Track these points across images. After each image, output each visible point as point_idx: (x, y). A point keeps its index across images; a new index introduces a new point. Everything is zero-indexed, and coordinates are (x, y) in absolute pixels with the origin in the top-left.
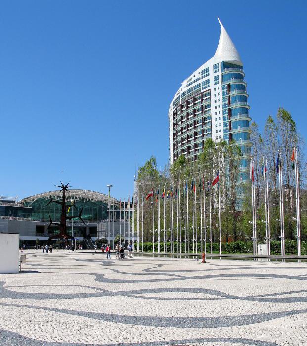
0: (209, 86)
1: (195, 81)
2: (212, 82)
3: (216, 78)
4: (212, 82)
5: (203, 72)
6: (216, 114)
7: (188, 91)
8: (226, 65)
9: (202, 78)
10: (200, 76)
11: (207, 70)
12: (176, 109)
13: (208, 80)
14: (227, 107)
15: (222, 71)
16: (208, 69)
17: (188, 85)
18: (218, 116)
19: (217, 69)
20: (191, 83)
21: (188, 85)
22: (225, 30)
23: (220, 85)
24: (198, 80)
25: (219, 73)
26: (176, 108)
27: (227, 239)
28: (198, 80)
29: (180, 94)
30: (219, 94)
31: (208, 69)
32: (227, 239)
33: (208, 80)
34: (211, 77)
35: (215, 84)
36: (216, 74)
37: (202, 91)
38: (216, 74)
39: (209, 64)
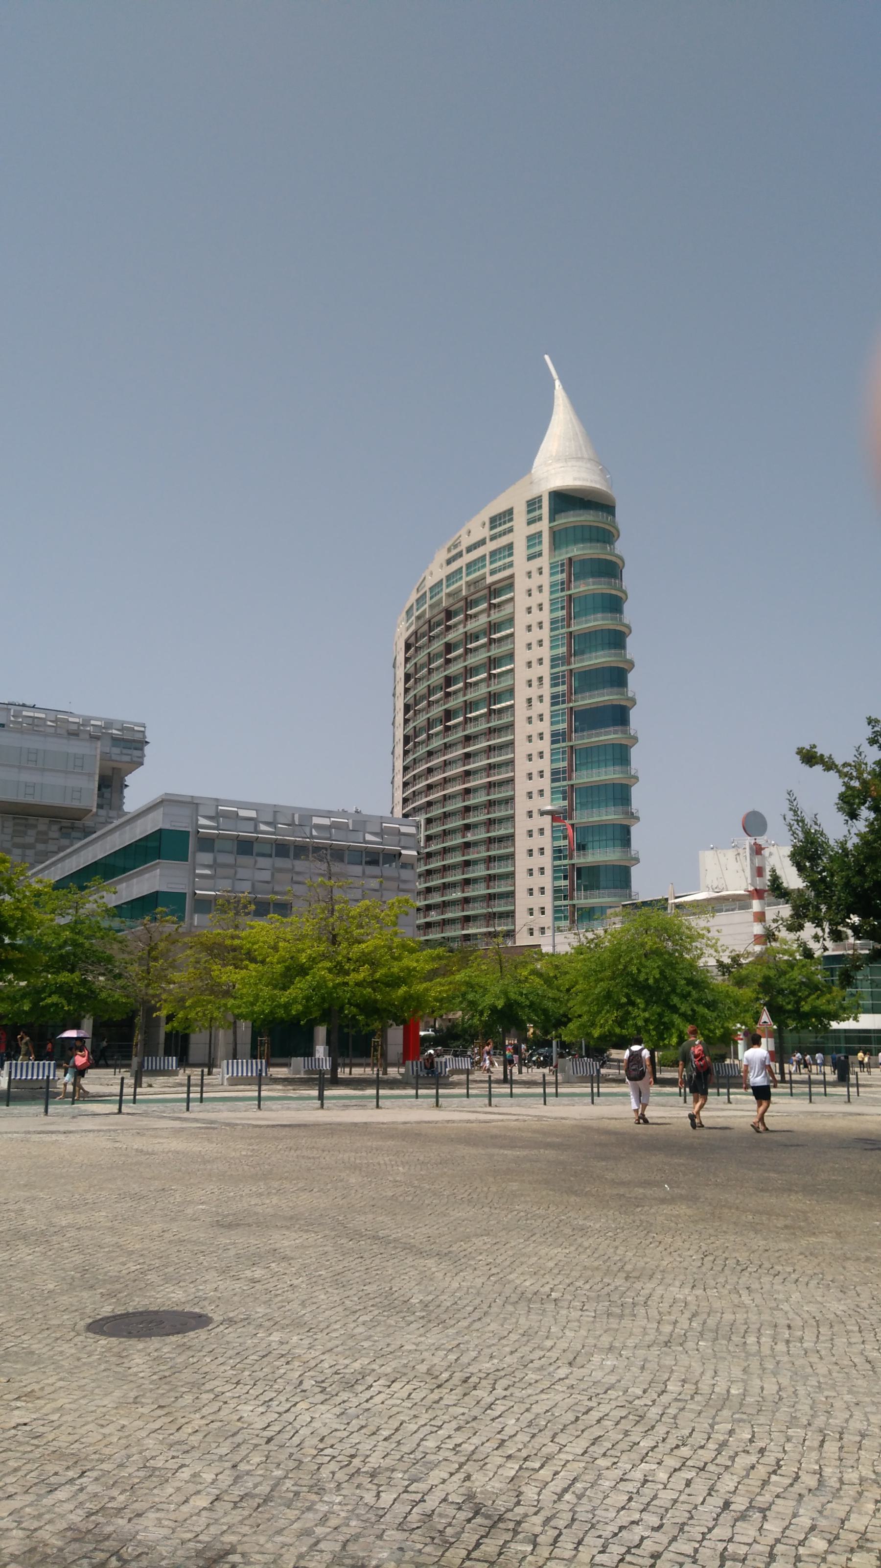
0: (511, 565)
1: (469, 549)
2: (520, 550)
3: (533, 539)
4: (520, 550)
5: (494, 521)
6: (529, 574)
7: (448, 577)
8: (564, 500)
9: (493, 538)
10: (486, 532)
11: (509, 514)
12: (416, 632)
13: (510, 546)
14: (563, 702)
15: (552, 519)
16: (510, 512)
17: (449, 562)
18: (537, 616)
19: (537, 513)
20: (460, 555)
21: (449, 562)
22: (566, 401)
23: (544, 561)
24: (482, 542)
25: (544, 526)
26: (413, 628)
27: (235, 1050)
28: (482, 542)
29: (427, 588)
30: (540, 662)
31: (510, 512)
32: (235, 1050)
33: (510, 546)
34: (521, 530)
35: (530, 558)
36: (534, 529)
37: (490, 580)
38: (534, 529)
39: (515, 498)
